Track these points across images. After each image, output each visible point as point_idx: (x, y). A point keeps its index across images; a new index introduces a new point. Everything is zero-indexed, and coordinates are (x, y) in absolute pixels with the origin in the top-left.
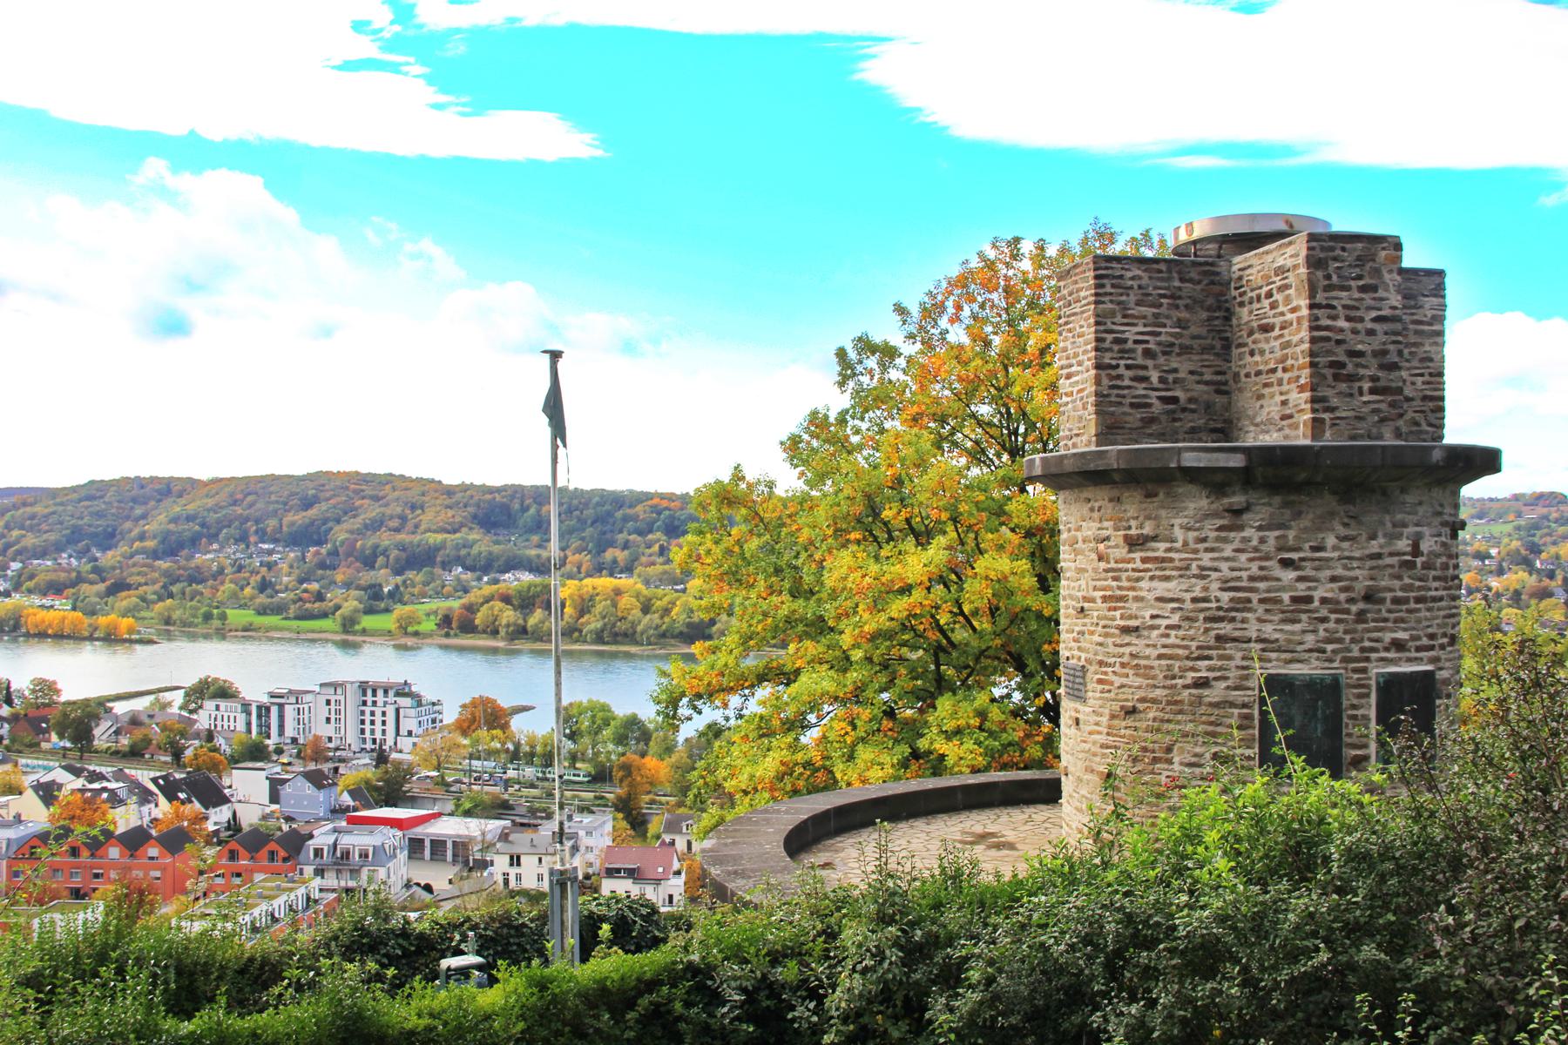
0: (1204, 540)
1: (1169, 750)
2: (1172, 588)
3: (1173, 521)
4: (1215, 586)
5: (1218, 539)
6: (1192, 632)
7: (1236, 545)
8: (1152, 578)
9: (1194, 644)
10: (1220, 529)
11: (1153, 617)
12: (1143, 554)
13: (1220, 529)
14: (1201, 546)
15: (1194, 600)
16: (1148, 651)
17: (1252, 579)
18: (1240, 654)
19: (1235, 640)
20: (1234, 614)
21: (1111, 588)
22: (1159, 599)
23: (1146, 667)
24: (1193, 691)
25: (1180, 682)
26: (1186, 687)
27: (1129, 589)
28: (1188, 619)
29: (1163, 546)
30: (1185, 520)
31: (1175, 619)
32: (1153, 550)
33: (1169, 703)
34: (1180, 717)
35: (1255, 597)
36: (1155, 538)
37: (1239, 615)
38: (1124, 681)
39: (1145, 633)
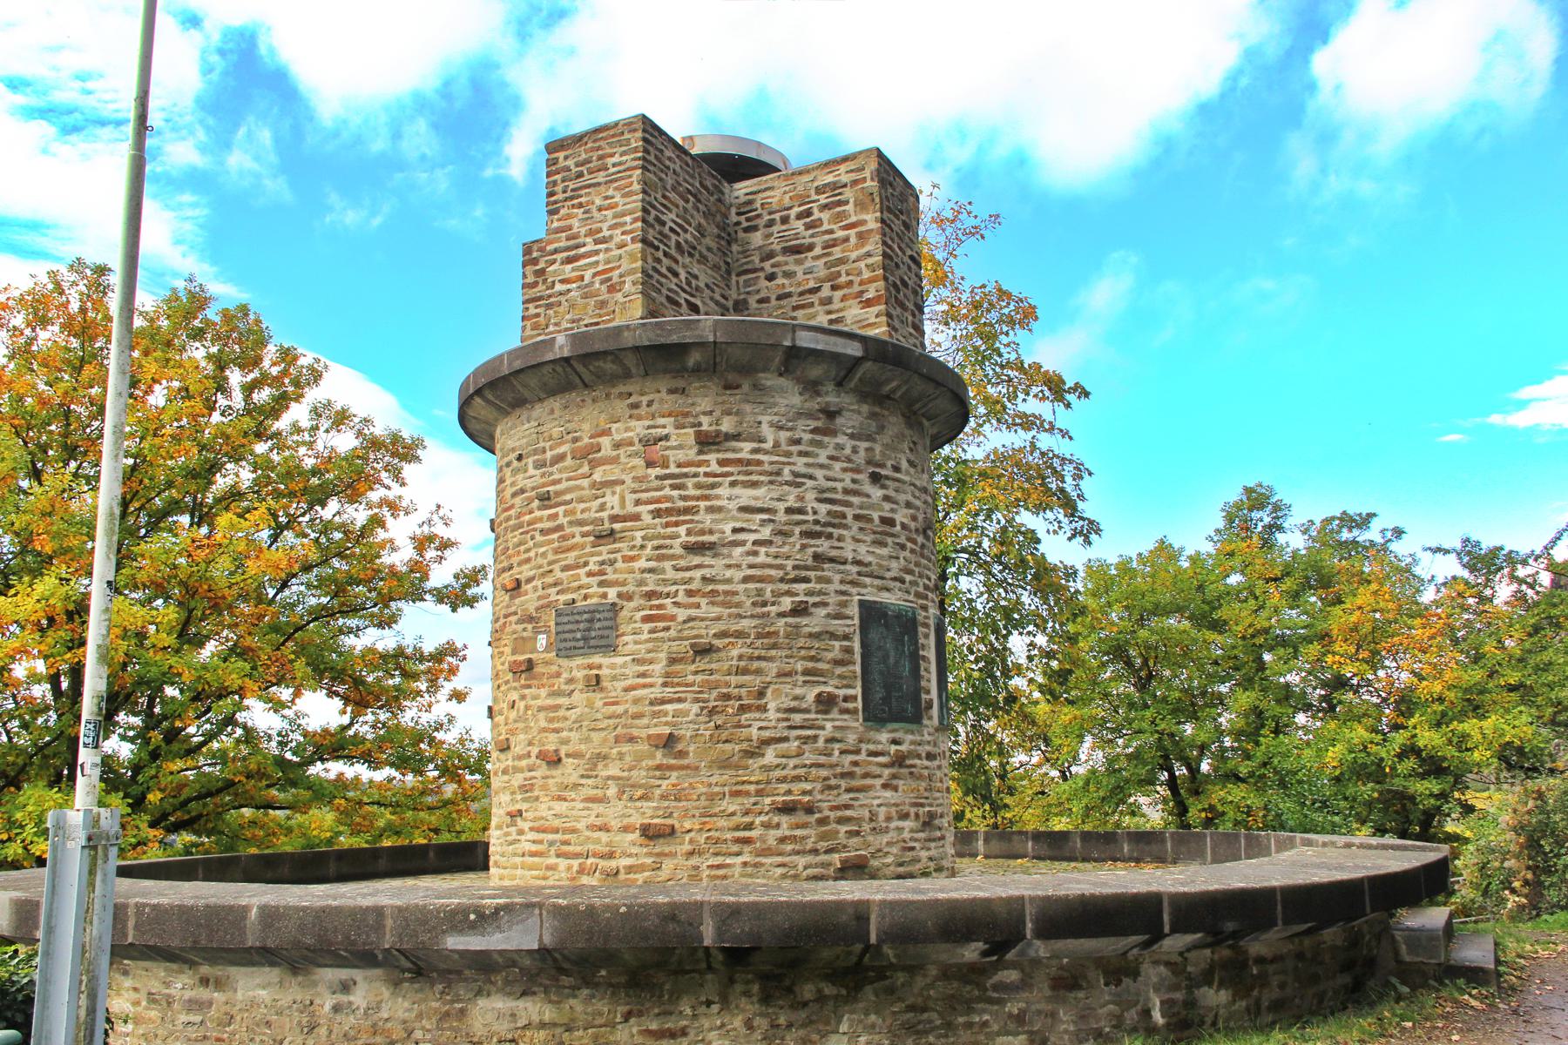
0: (798, 442)
1: (761, 694)
2: (761, 495)
3: (760, 418)
4: (811, 496)
5: (812, 443)
6: (786, 549)
7: (830, 451)
8: (733, 484)
9: (790, 564)
10: (815, 431)
11: (735, 531)
12: (721, 456)
13: (815, 431)
14: (794, 449)
15: (789, 511)
16: (728, 574)
17: (846, 491)
18: (837, 577)
19: (832, 560)
20: (830, 530)
21: (669, 499)
22: (743, 509)
23: (726, 593)
24: (790, 620)
25: (773, 609)
26: (782, 615)
27: (698, 499)
28: (781, 533)
29: (748, 446)
30: (774, 416)
31: (766, 533)
32: (734, 451)
33: (759, 636)
34: (773, 652)
35: (850, 512)
36: (737, 437)
37: (836, 532)
38: (693, 612)
39: (725, 551)
